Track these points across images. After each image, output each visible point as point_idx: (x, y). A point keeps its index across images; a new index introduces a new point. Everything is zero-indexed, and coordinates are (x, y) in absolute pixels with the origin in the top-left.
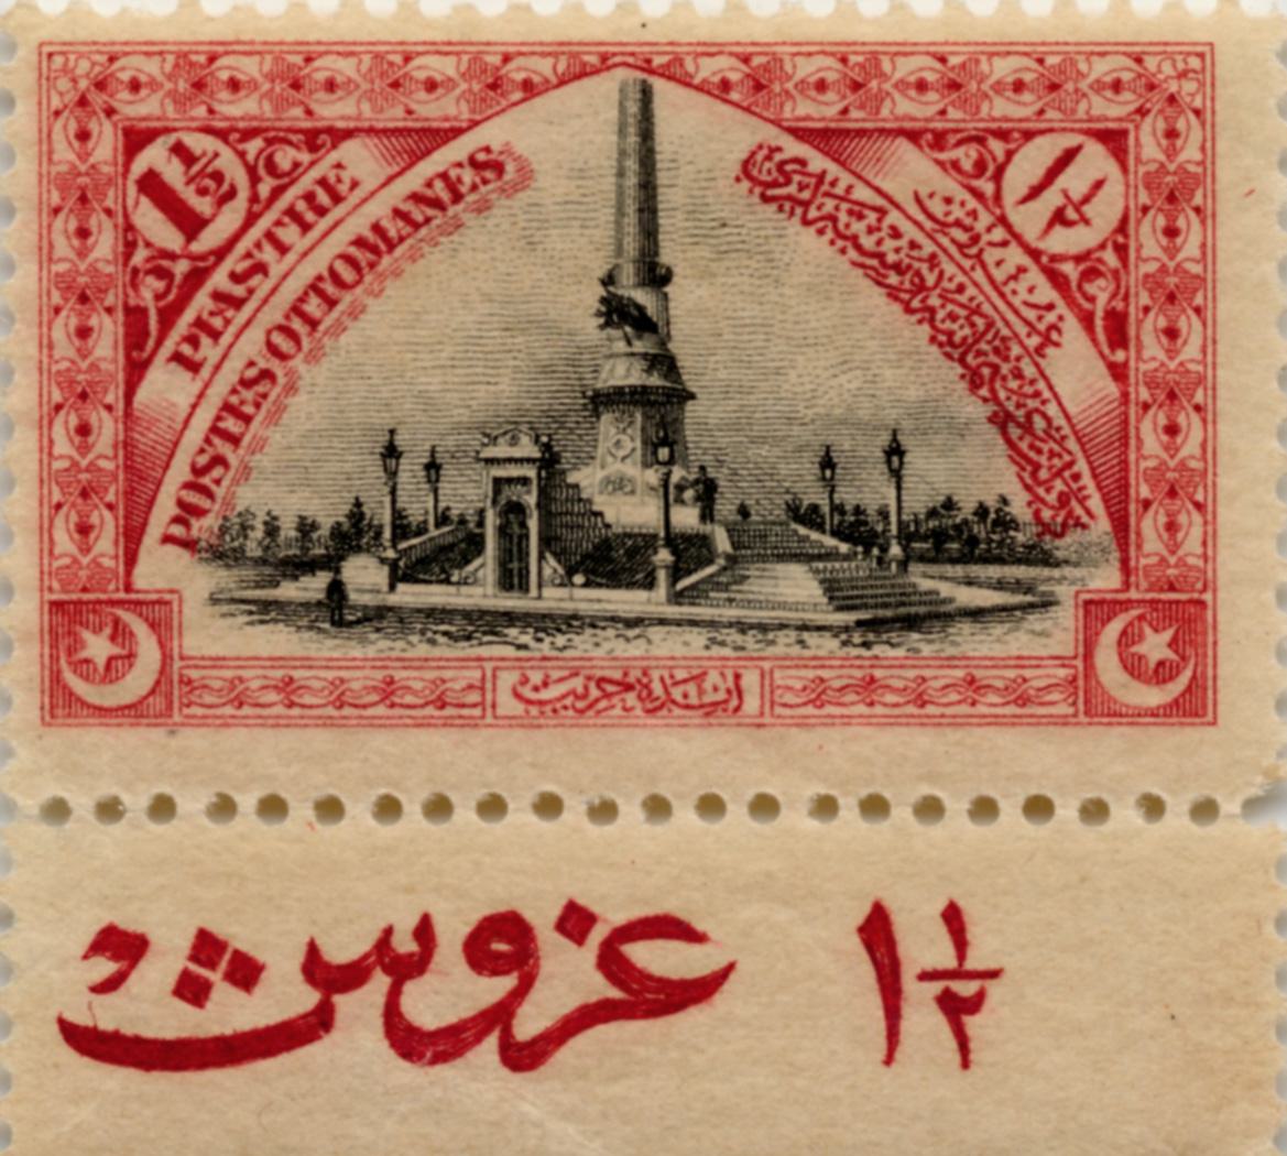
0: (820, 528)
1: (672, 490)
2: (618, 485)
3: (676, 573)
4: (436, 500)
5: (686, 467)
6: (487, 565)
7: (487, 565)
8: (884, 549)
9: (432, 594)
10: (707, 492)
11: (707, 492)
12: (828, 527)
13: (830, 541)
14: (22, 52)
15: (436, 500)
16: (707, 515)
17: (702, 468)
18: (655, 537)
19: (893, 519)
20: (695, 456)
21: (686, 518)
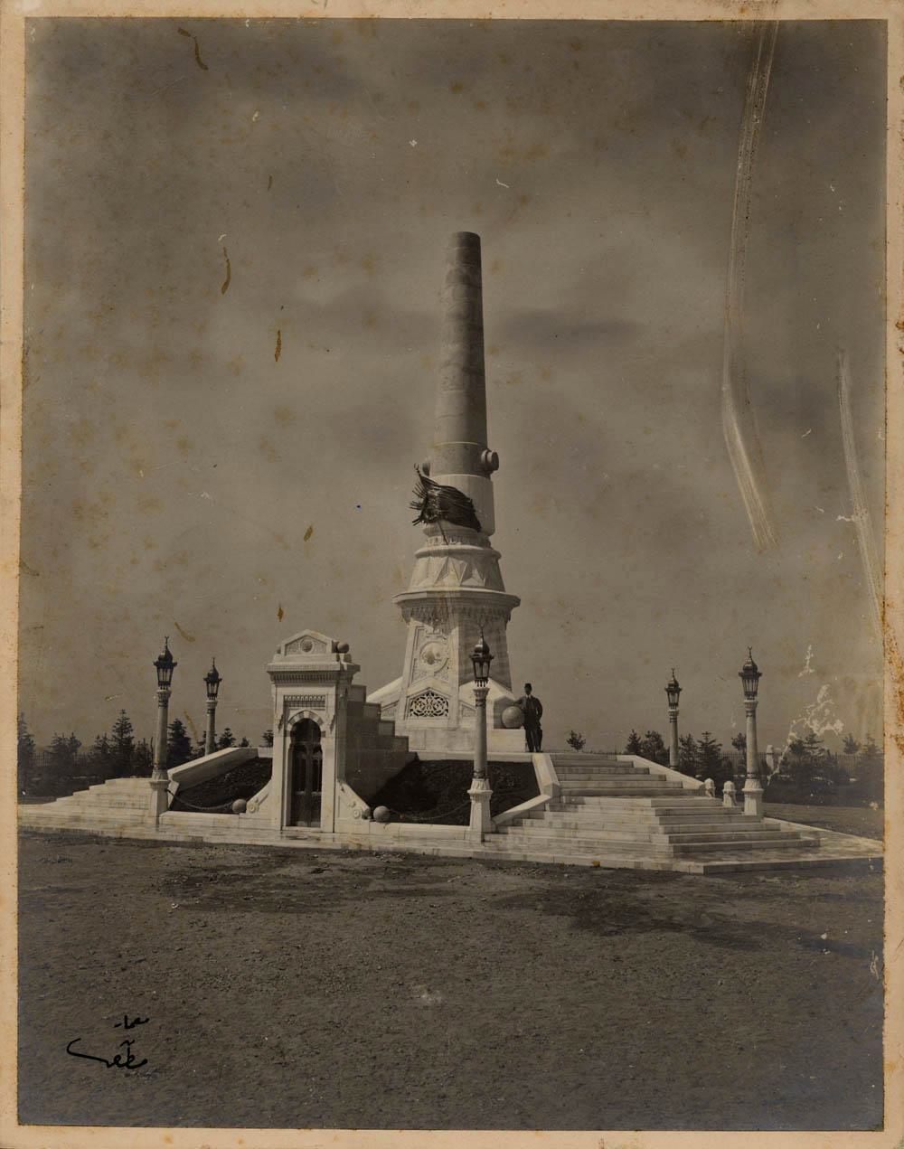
0: (663, 761)
1: (490, 708)
2: (428, 704)
3: (496, 807)
4: (165, 714)
5: (506, 685)
6: (272, 798)
7: (272, 798)
8: (739, 784)
9: (314, 832)
10: (529, 716)
11: (529, 716)
12: (672, 762)
13: (674, 776)
14: (889, 735)
15: (165, 714)
16: (534, 742)
17: (528, 687)
18: (469, 764)
19: (749, 750)
20: (518, 676)
21: (509, 745)
